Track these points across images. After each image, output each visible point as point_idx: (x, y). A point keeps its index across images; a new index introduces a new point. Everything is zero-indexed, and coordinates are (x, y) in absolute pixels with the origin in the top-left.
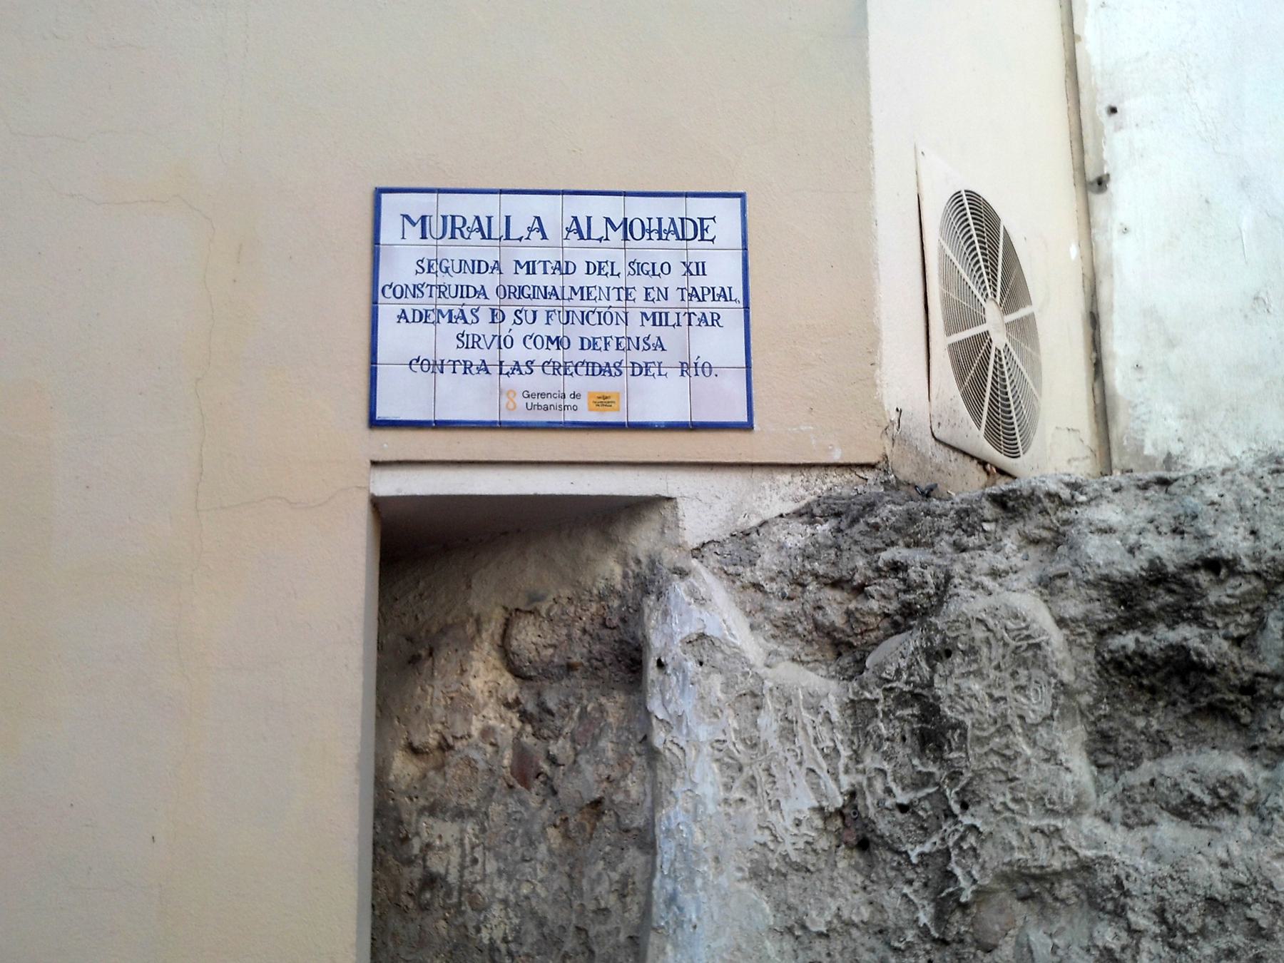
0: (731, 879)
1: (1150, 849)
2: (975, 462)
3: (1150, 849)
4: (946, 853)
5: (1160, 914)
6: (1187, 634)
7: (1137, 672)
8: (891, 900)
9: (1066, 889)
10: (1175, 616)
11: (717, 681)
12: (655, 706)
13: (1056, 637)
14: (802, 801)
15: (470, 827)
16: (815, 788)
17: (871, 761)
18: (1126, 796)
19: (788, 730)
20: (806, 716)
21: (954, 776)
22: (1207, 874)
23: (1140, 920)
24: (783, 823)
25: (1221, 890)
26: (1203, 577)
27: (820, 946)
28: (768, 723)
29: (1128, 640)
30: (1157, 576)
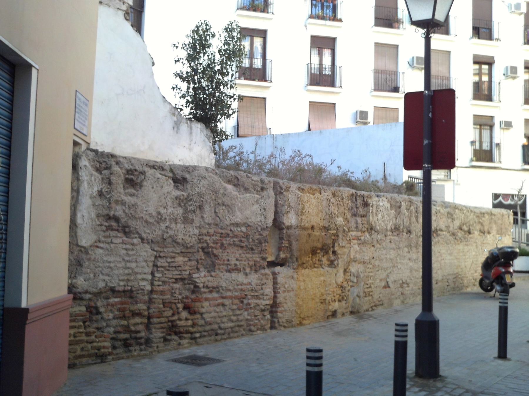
0: (88, 197)
1: (128, 199)
2: (261, 393)
3: (128, 199)
4: (110, 197)
5: (129, 206)
6: (132, 177)
7: (370, 233)
8: (104, 202)
9: (120, 202)
10: (131, 175)
11: (87, 172)
12: (80, 173)
13: (122, 174)
14: (96, 189)
15: (155, 320)
16: (98, 187)
17: (104, 185)
18: (125, 193)
19: (95, 180)
20: (97, 179)
21: (112, 188)
22: (133, 202)
23: (127, 206)
24: (94, 191)
25: (134, 204)
26: (134, 171)
27: (96, 207)
28: (93, 178)
29: (127, 176)
30: (131, 170)
